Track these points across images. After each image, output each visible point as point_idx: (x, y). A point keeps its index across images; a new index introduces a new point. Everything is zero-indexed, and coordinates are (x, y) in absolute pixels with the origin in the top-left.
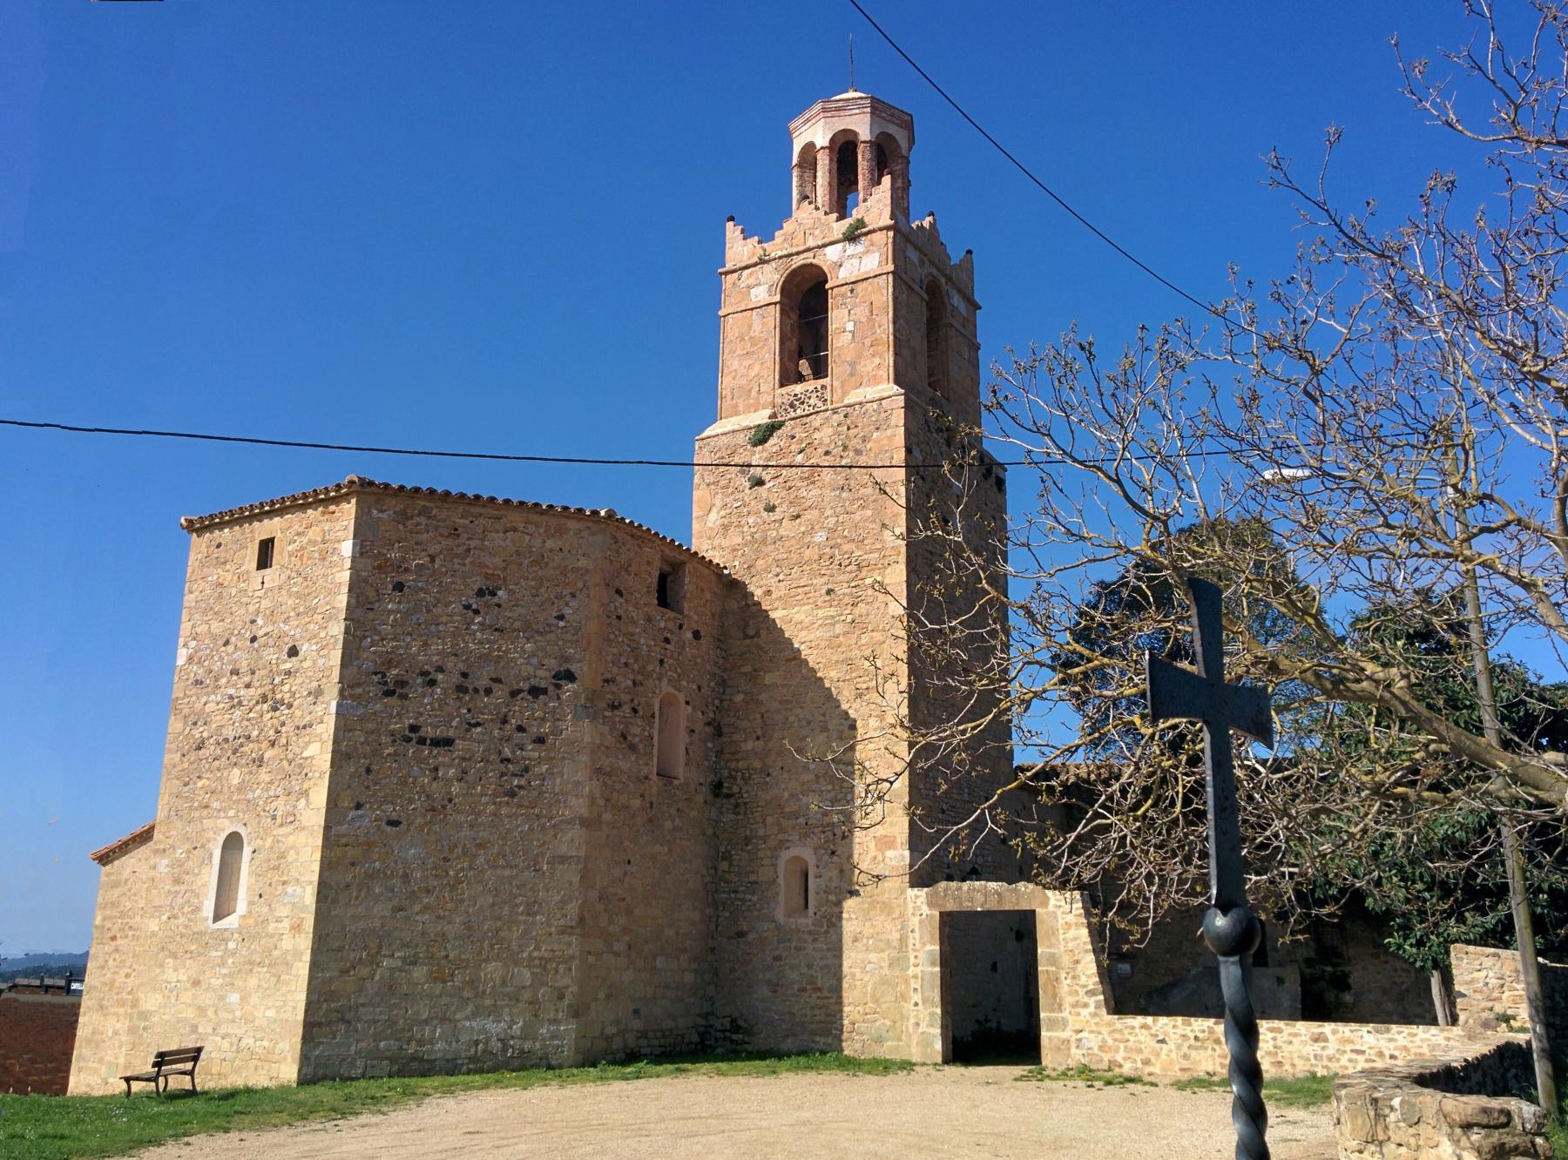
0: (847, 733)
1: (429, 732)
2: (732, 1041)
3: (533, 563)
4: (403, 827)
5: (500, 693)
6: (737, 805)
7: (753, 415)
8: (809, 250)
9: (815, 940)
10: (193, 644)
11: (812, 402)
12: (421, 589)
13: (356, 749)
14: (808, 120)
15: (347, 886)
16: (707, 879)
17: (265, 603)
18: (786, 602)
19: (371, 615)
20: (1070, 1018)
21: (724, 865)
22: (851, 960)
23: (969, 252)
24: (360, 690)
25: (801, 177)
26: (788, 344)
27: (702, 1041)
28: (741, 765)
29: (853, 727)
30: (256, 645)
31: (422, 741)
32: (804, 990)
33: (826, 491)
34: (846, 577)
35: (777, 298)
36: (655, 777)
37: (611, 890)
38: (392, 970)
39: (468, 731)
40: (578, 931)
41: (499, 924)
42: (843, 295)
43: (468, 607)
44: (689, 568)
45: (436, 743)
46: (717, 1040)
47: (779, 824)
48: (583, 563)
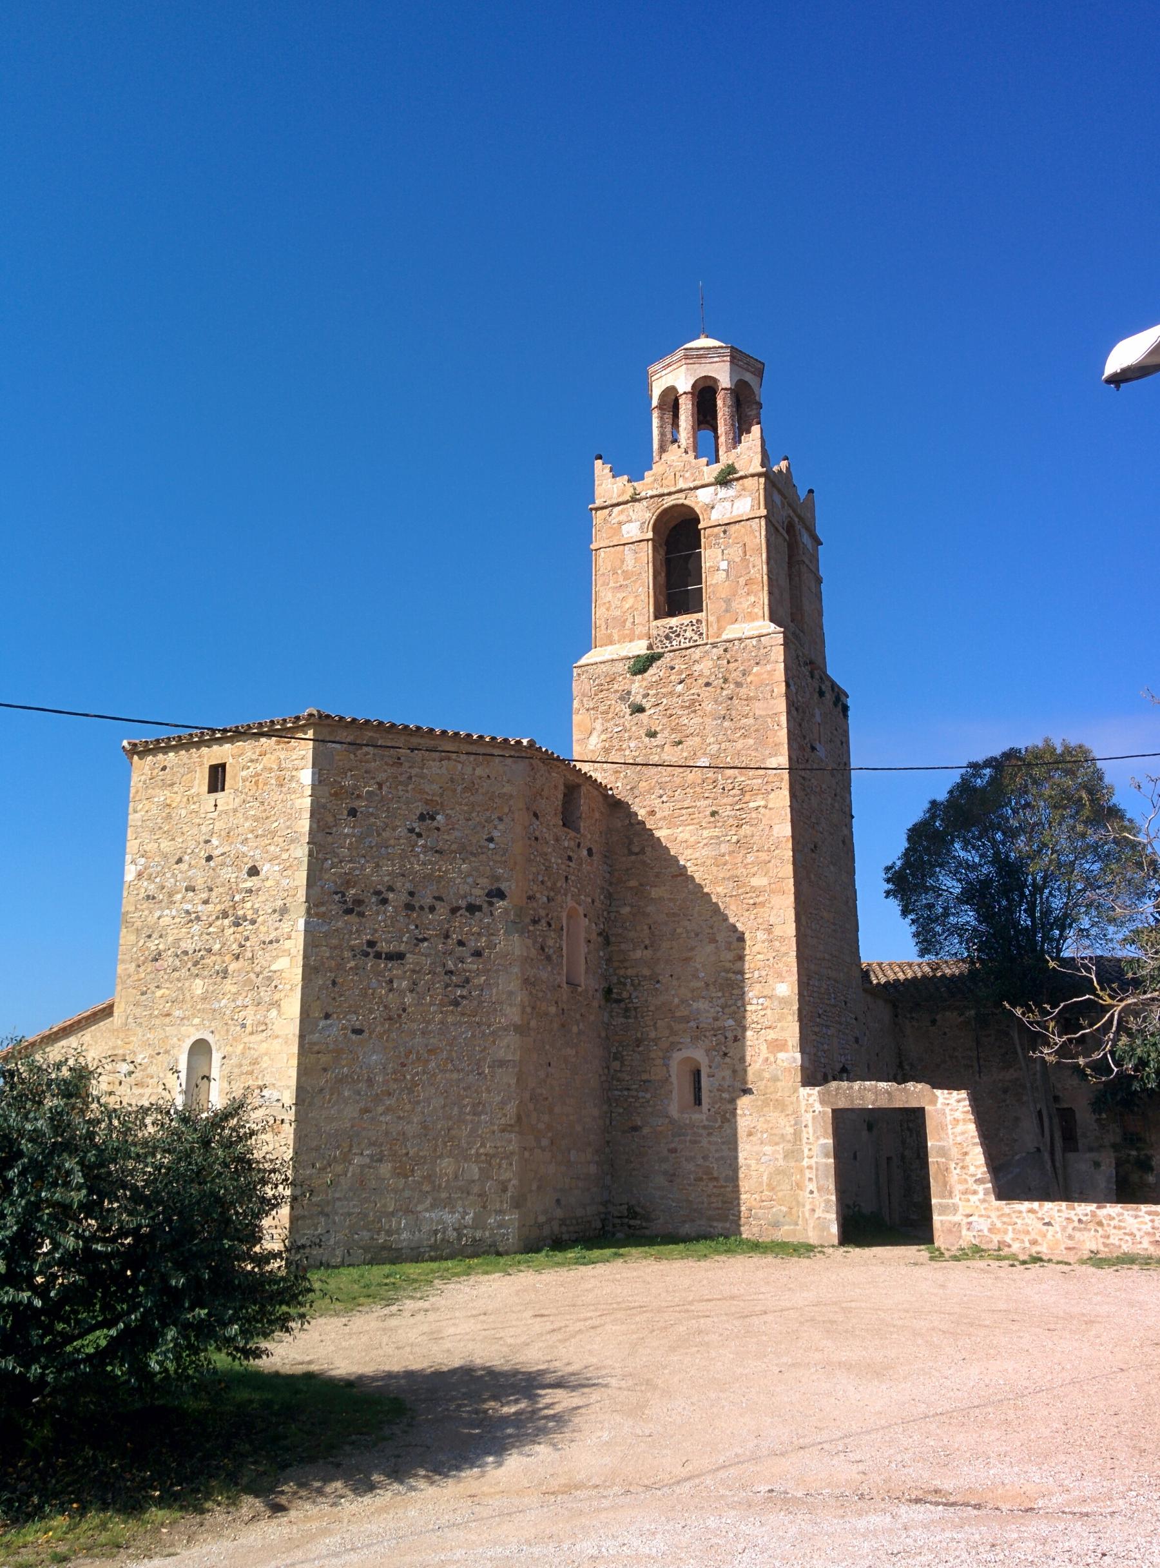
0: (735, 944)
1: (383, 947)
2: (630, 1227)
3: (466, 789)
4: (366, 1035)
5: (442, 910)
6: (627, 1010)
7: (629, 645)
8: (681, 491)
9: (710, 1134)
10: (143, 860)
11: (688, 635)
12: (372, 814)
13: (323, 964)
14: (669, 365)
15: (322, 1090)
16: (604, 1078)
17: (219, 825)
18: (671, 822)
19: (330, 839)
20: (960, 1203)
21: (616, 1065)
22: (746, 1152)
23: (811, 491)
24: (323, 909)
25: (661, 418)
26: (659, 578)
27: (603, 1227)
28: (630, 972)
29: (741, 939)
30: (212, 863)
31: (378, 956)
32: (701, 1179)
33: (708, 720)
34: (730, 800)
35: (650, 535)
36: (565, 985)
37: (539, 1091)
38: (362, 1166)
39: (416, 945)
40: (517, 1129)
41: (450, 1123)
42: (717, 536)
43: (411, 831)
44: (583, 789)
45: (390, 957)
46: (614, 1226)
47: (670, 1027)
48: (507, 789)
